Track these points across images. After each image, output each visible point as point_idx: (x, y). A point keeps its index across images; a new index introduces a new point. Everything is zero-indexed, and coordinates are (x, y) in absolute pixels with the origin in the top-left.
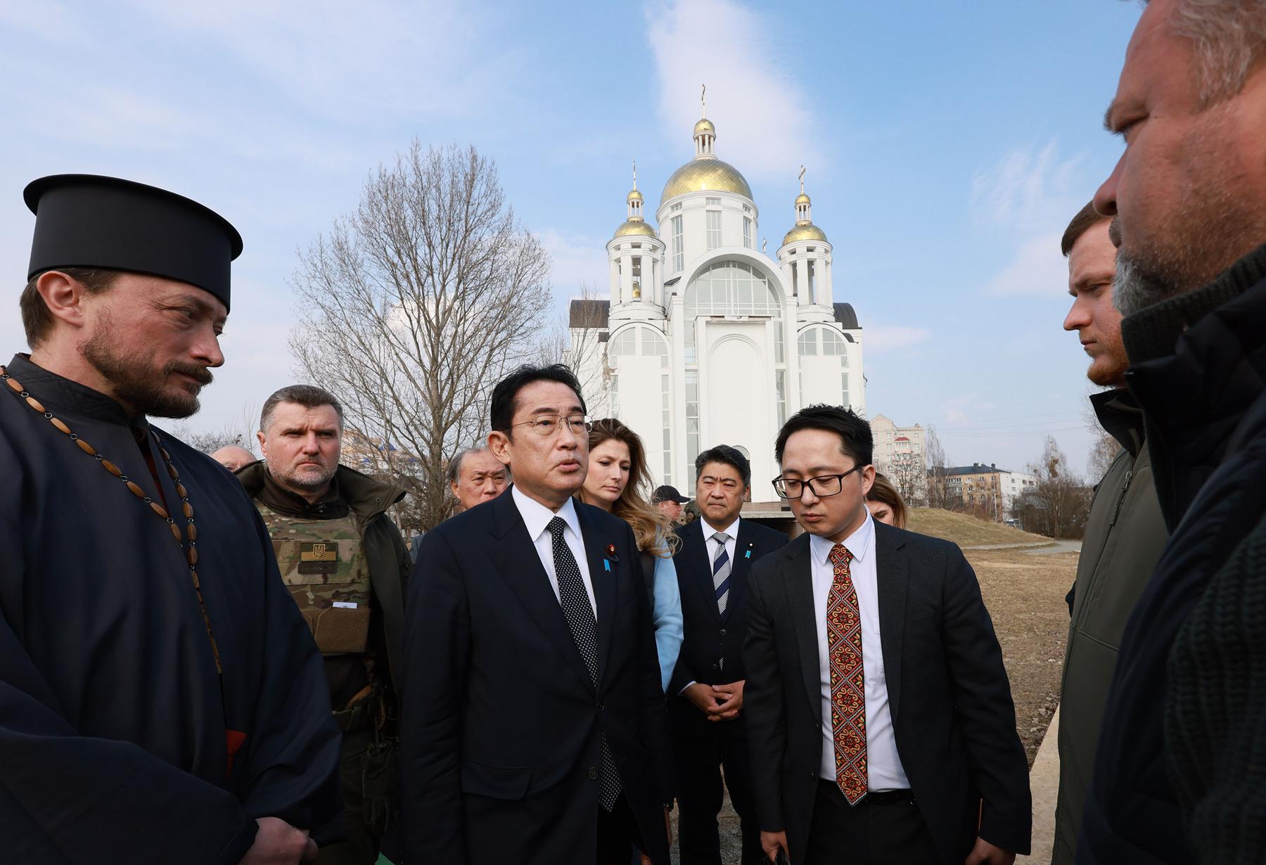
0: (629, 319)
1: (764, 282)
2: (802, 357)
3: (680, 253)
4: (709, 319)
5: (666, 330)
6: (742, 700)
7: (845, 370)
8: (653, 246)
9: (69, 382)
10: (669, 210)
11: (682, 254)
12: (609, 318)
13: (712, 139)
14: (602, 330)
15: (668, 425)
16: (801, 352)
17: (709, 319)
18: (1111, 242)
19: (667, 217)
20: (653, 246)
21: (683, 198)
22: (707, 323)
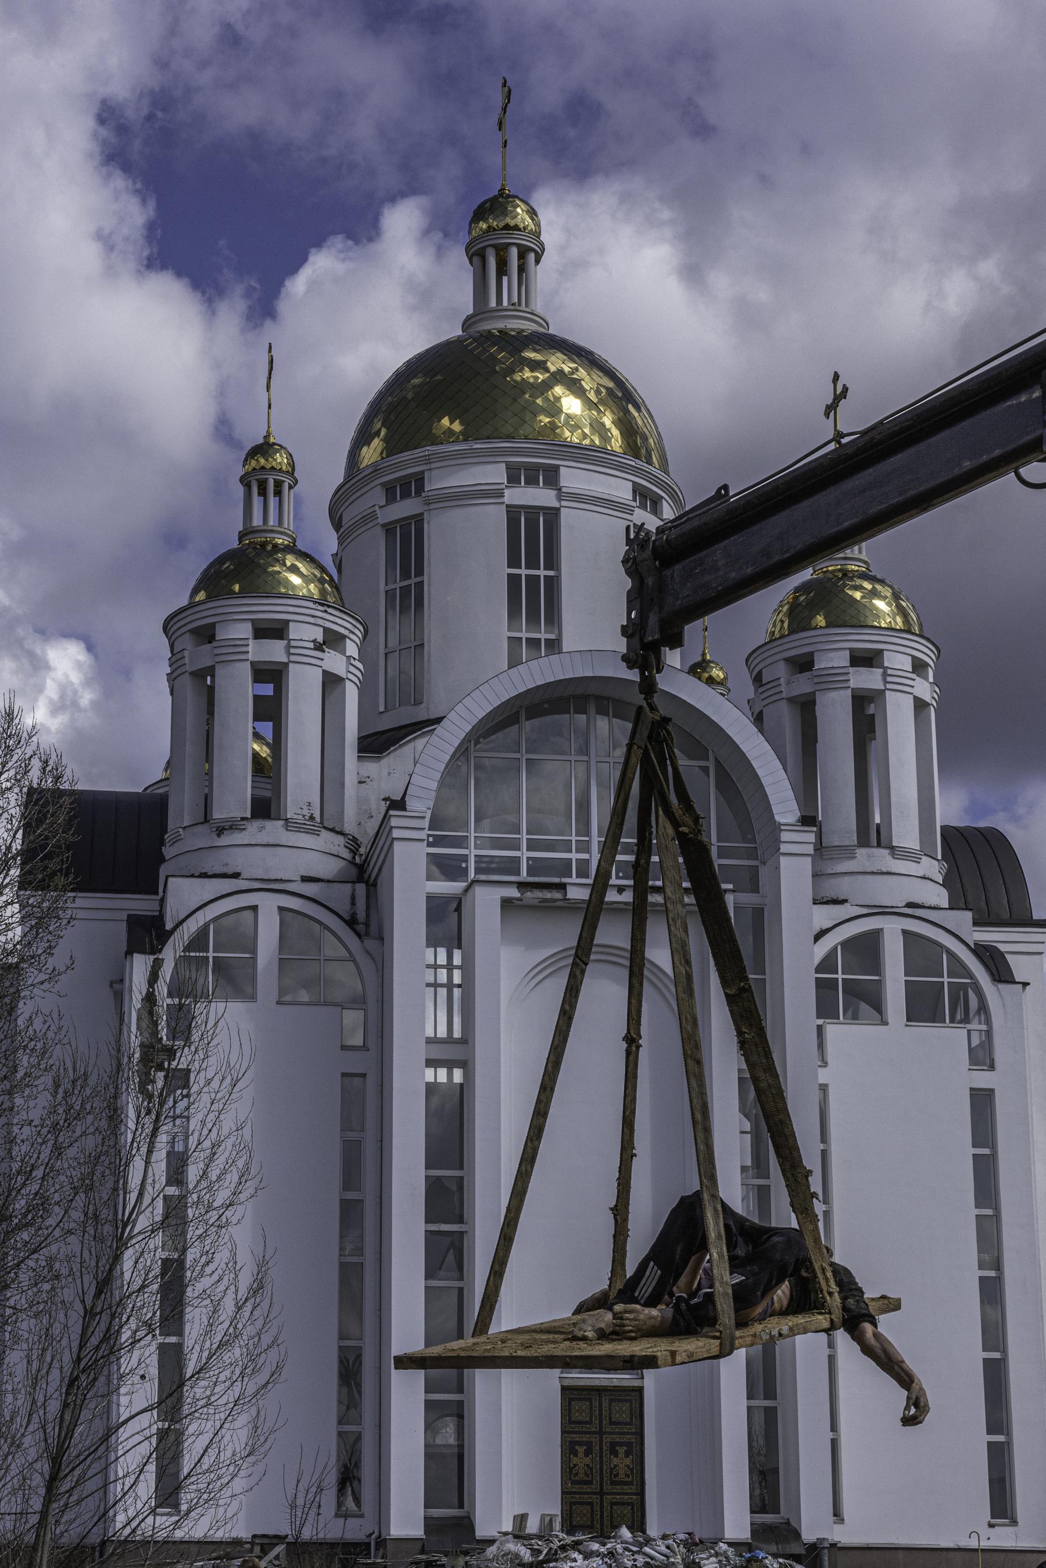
0: (236, 875)
1: (705, 770)
2: (833, 1031)
3: (413, 581)
4: (514, 893)
5: (361, 916)
6: (331, 240)
7: (983, 1079)
8: (326, 630)
9: (488, 1320)
10: (378, 496)
11: (420, 584)
12: (164, 870)
13: (532, 256)
14: (141, 904)
15: (360, 1251)
16: (826, 1009)
17: (514, 893)
18: (417, 1350)
19: (371, 516)
20: (326, 630)
21: (427, 459)
22: (507, 903)
